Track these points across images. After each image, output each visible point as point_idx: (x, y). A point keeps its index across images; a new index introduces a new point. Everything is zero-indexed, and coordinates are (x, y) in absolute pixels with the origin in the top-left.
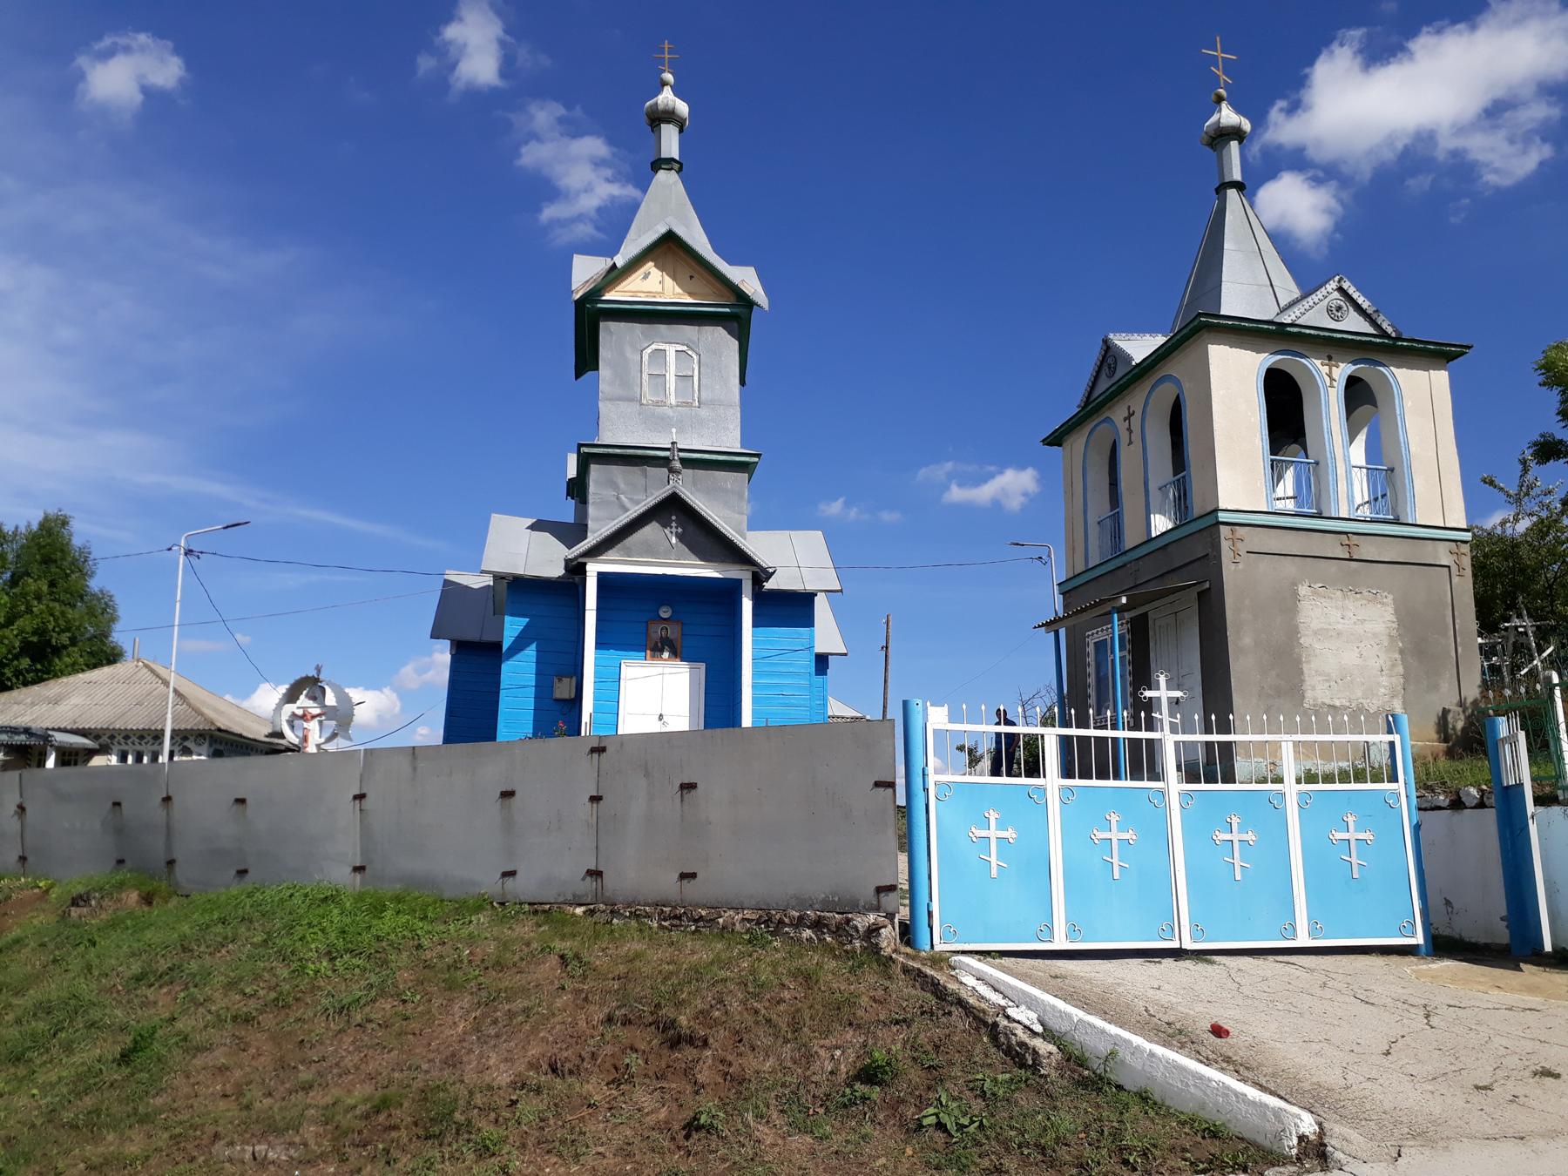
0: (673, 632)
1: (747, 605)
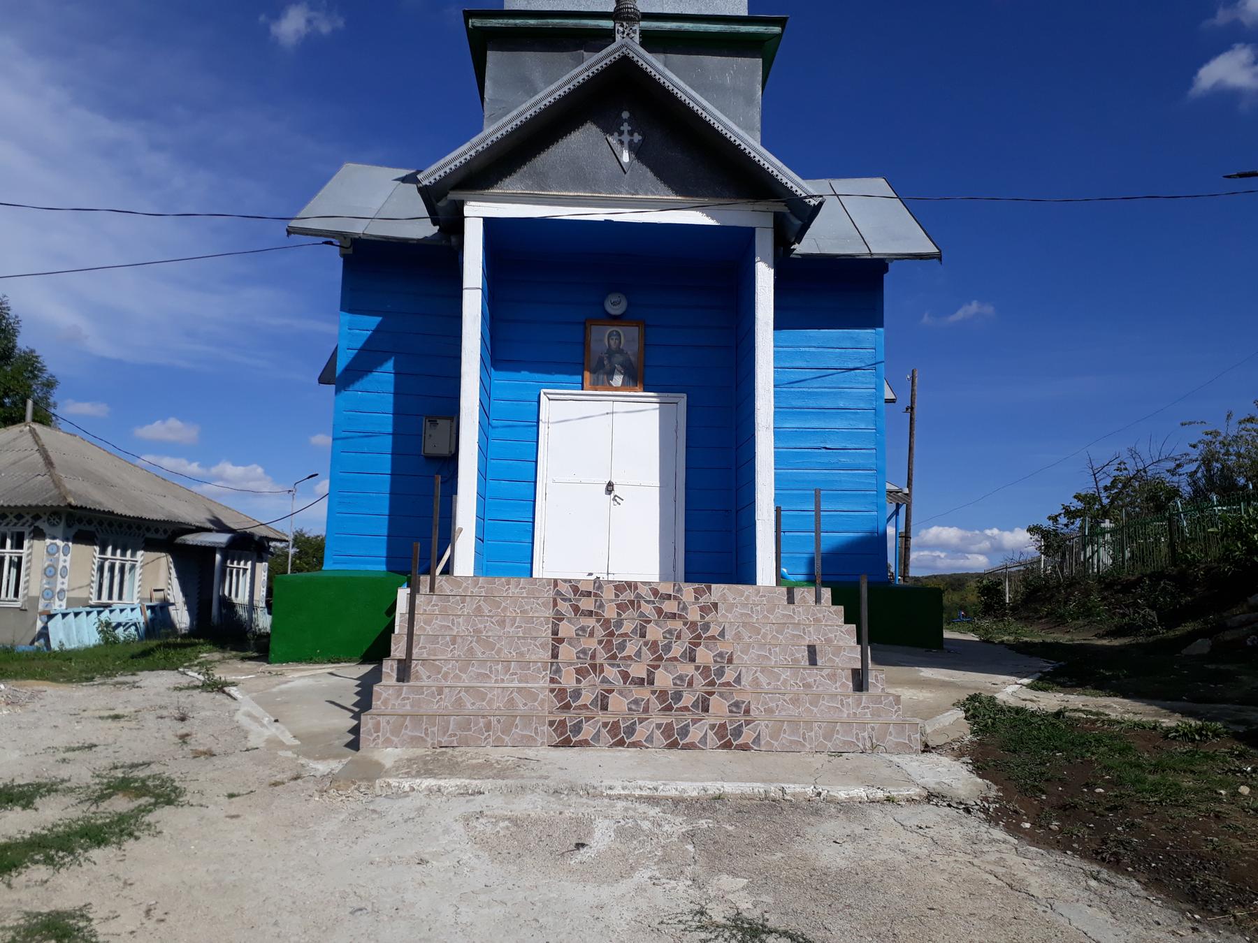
0: (628, 338)
1: (765, 276)
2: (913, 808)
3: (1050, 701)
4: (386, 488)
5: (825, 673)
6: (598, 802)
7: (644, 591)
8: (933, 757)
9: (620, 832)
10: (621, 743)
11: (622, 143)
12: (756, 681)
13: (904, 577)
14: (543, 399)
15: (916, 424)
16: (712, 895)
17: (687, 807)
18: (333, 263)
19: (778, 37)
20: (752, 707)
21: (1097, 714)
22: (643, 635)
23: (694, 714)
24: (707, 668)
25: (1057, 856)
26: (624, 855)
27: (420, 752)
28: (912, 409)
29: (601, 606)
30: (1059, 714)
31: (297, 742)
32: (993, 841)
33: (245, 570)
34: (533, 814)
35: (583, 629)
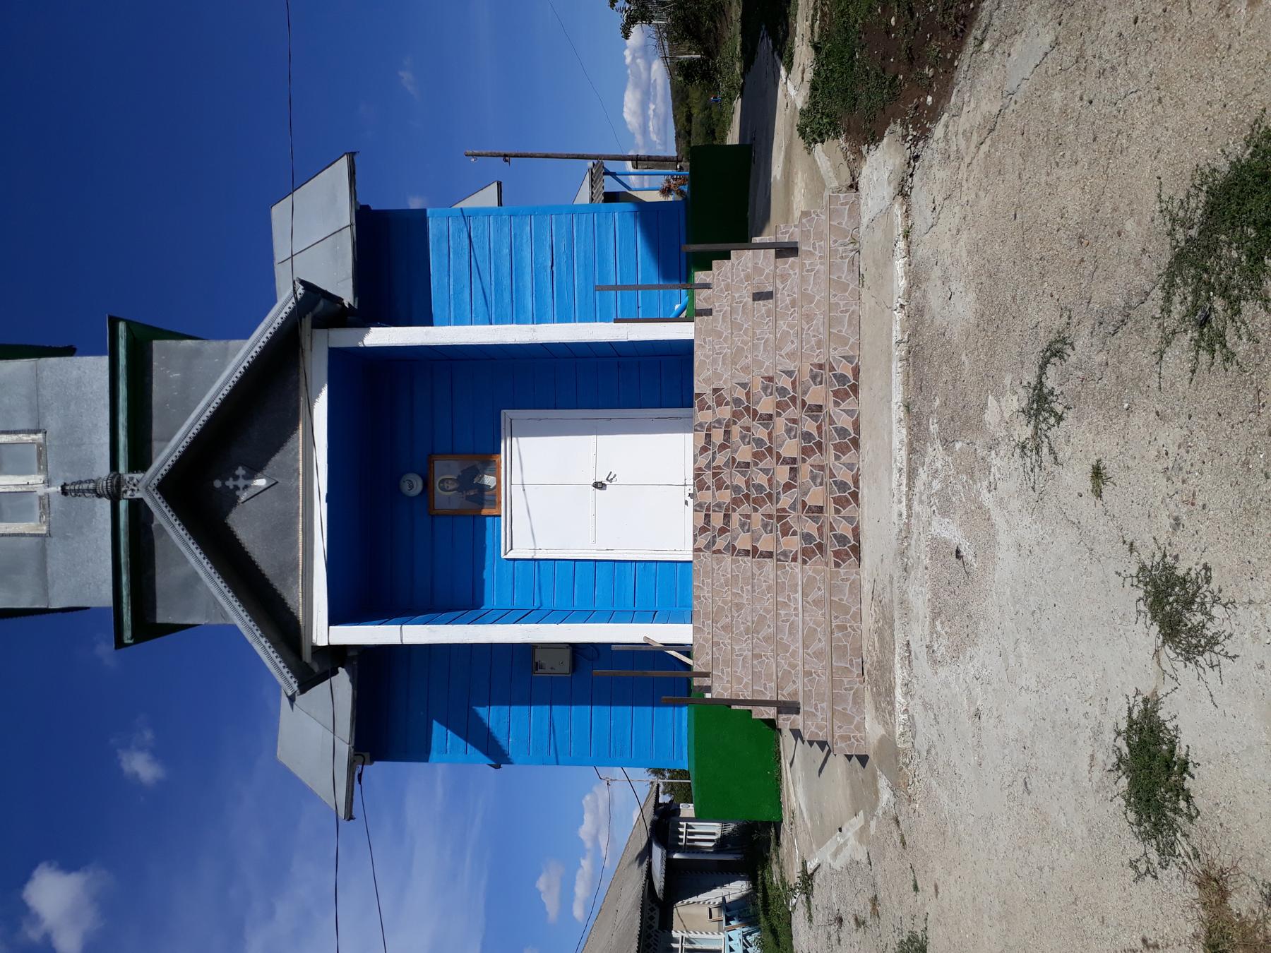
0: (446, 471)
1: (379, 337)
2: (914, 212)
3: (803, 54)
4: (606, 709)
5: (780, 286)
6: (914, 529)
7: (703, 461)
8: (862, 182)
9: (944, 513)
10: (855, 495)
11: (246, 487)
12: (790, 356)
13: (678, 161)
14: (511, 555)
15: (522, 151)
16: (1005, 433)
17: (918, 441)
18: (377, 771)
19: (129, 324)
20: (816, 361)
21: (815, 9)
22: (747, 465)
23: (824, 420)
24: (778, 405)
25: (960, 75)
26: (966, 513)
27: (868, 696)
28: (505, 156)
29: (719, 505)
30: (817, 48)
31: (861, 813)
32: (946, 138)
33: (688, 826)
34: (928, 596)
35: (742, 525)
